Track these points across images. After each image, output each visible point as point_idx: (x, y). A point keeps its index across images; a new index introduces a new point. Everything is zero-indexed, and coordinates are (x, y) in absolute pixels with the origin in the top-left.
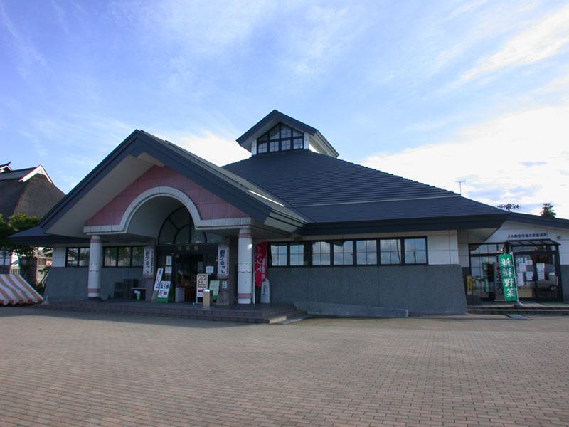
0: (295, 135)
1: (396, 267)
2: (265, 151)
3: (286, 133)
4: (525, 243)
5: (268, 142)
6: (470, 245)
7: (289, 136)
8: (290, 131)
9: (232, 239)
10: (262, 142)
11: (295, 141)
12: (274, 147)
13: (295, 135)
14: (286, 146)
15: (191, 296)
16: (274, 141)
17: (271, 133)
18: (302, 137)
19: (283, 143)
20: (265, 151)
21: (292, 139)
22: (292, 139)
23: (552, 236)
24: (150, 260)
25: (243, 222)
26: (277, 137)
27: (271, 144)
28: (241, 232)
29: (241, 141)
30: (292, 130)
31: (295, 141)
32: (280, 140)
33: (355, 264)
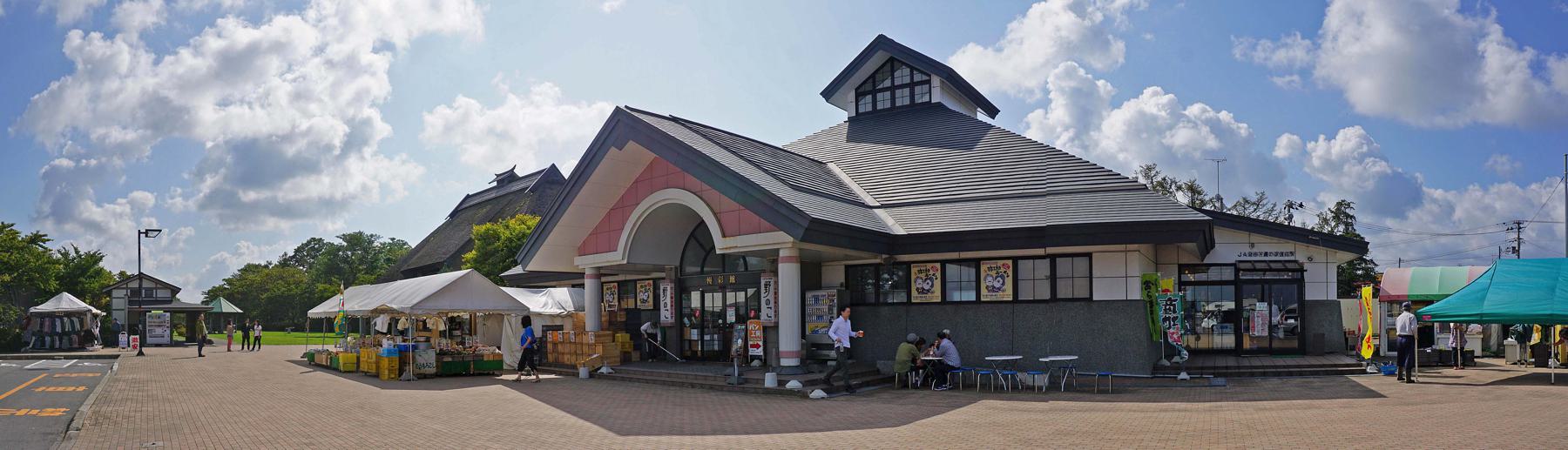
0: (918, 77)
1: (1042, 306)
2: (869, 108)
3: (902, 76)
4: (1258, 266)
5: (874, 92)
6: (1180, 266)
7: (907, 80)
8: (907, 71)
9: (771, 259)
10: (865, 94)
11: (918, 89)
12: (884, 101)
13: (918, 77)
14: (903, 98)
15: (915, 369)
16: (902, 86)
17: (879, 77)
18: (928, 82)
19: (898, 93)
20: (869, 108)
21: (912, 85)
22: (912, 85)
23: (1301, 256)
24: (668, 301)
25: (782, 240)
26: (888, 83)
27: (879, 96)
28: (782, 253)
29: (828, 94)
30: (912, 69)
31: (918, 89)
32: (893, 89)
33: (1054, 298)
